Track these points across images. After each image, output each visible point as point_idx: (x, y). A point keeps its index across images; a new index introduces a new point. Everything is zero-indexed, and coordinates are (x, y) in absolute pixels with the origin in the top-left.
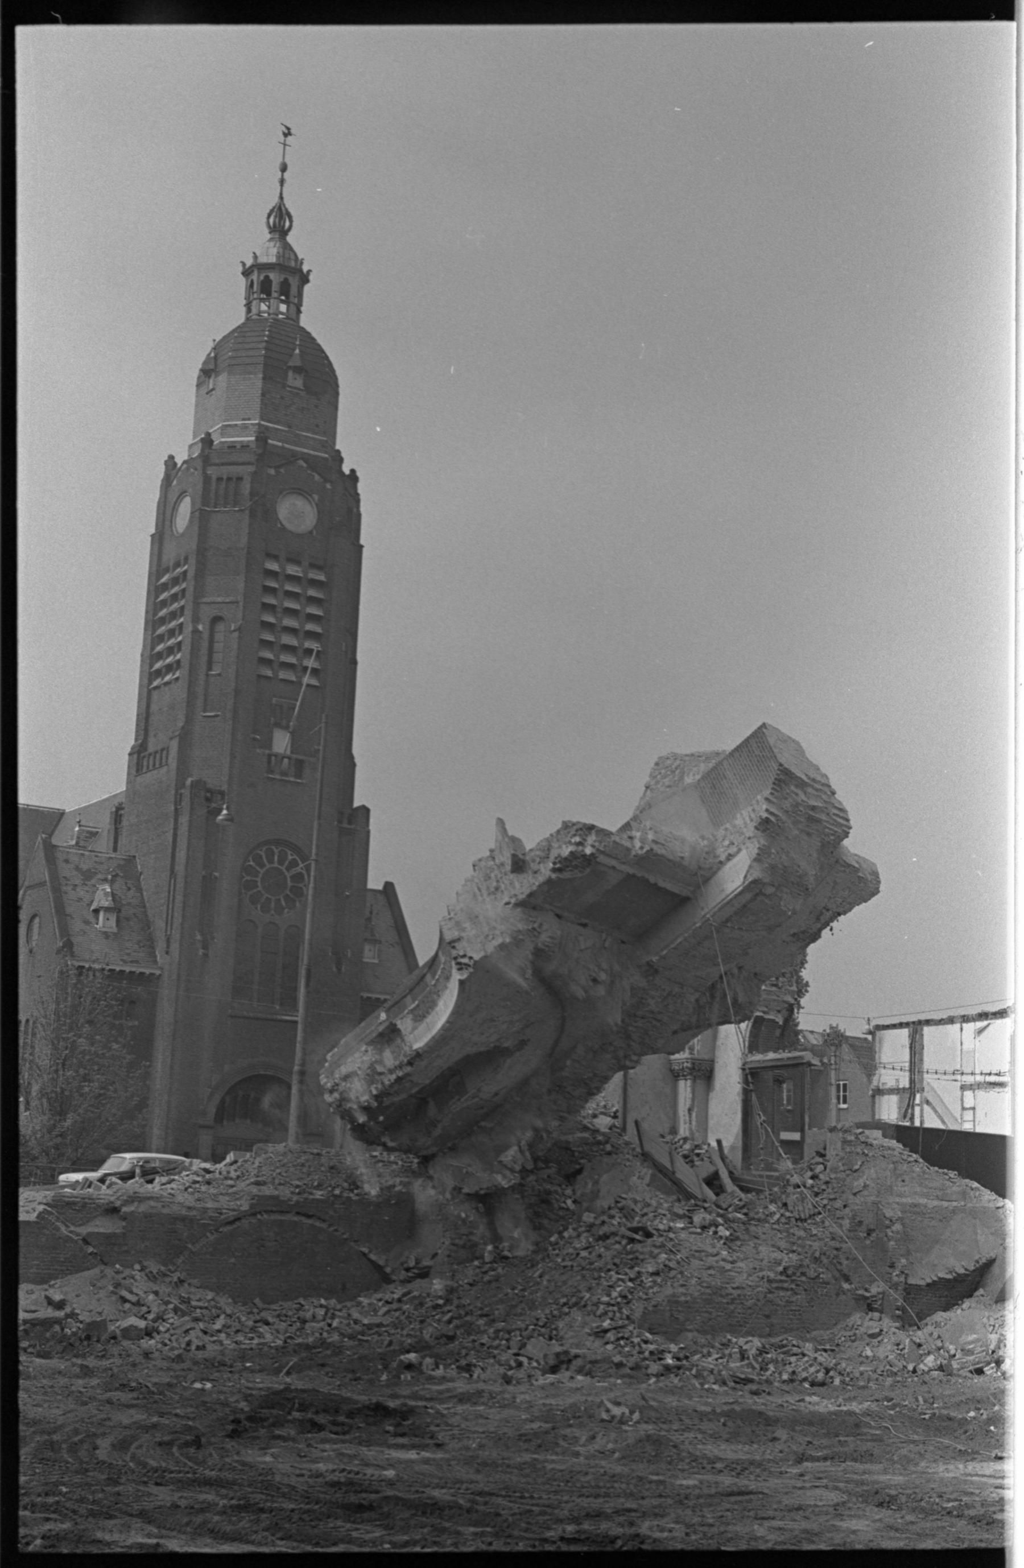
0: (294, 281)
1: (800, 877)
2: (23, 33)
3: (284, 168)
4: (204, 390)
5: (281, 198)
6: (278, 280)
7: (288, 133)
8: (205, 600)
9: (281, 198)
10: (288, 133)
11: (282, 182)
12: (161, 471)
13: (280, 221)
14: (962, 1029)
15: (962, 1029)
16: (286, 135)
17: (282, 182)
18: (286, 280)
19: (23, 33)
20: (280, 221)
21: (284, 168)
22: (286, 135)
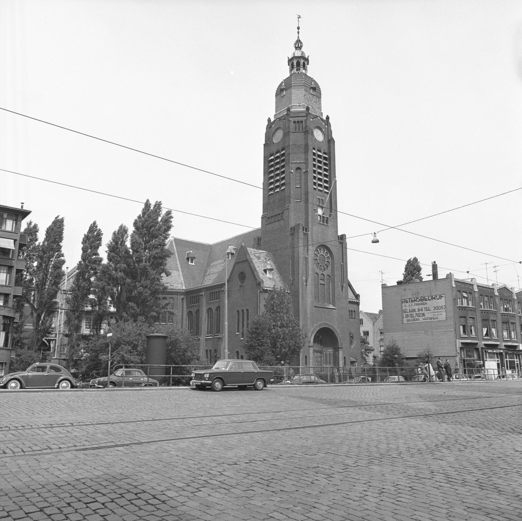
0: (302, 61)
1: (155, 293)
2: (439, 278)
3: (298, 28)
4: (279, 97)
5: (298, 37)
6: (298, 63)
7: (299, 17)
8: (430, 365)
9: (298, 37)
10: (299, 17)
11: (298, 33)
12: (266, 123)
13: (298, 45)
14: (429, 275)
15: (429, 275)
16: (299, 18)
17: (298, 33)
18: (298, 61)
19: (439, 278)
20: (298, 45)
21: (298, 28)
22: (299, 18)
